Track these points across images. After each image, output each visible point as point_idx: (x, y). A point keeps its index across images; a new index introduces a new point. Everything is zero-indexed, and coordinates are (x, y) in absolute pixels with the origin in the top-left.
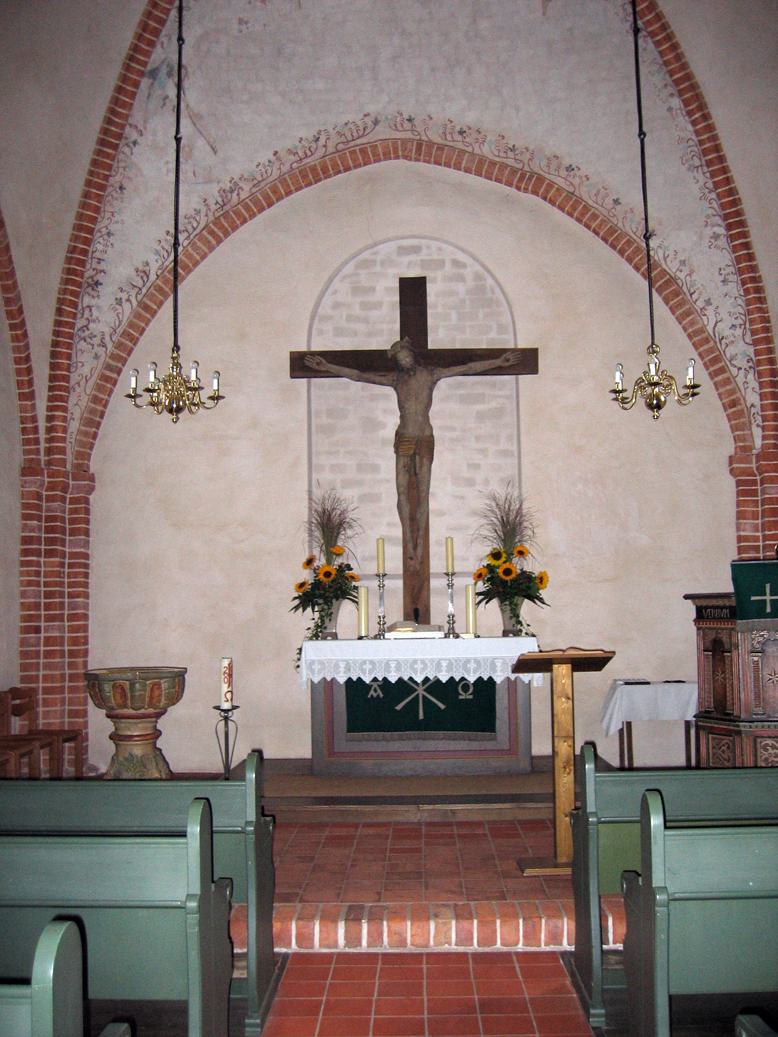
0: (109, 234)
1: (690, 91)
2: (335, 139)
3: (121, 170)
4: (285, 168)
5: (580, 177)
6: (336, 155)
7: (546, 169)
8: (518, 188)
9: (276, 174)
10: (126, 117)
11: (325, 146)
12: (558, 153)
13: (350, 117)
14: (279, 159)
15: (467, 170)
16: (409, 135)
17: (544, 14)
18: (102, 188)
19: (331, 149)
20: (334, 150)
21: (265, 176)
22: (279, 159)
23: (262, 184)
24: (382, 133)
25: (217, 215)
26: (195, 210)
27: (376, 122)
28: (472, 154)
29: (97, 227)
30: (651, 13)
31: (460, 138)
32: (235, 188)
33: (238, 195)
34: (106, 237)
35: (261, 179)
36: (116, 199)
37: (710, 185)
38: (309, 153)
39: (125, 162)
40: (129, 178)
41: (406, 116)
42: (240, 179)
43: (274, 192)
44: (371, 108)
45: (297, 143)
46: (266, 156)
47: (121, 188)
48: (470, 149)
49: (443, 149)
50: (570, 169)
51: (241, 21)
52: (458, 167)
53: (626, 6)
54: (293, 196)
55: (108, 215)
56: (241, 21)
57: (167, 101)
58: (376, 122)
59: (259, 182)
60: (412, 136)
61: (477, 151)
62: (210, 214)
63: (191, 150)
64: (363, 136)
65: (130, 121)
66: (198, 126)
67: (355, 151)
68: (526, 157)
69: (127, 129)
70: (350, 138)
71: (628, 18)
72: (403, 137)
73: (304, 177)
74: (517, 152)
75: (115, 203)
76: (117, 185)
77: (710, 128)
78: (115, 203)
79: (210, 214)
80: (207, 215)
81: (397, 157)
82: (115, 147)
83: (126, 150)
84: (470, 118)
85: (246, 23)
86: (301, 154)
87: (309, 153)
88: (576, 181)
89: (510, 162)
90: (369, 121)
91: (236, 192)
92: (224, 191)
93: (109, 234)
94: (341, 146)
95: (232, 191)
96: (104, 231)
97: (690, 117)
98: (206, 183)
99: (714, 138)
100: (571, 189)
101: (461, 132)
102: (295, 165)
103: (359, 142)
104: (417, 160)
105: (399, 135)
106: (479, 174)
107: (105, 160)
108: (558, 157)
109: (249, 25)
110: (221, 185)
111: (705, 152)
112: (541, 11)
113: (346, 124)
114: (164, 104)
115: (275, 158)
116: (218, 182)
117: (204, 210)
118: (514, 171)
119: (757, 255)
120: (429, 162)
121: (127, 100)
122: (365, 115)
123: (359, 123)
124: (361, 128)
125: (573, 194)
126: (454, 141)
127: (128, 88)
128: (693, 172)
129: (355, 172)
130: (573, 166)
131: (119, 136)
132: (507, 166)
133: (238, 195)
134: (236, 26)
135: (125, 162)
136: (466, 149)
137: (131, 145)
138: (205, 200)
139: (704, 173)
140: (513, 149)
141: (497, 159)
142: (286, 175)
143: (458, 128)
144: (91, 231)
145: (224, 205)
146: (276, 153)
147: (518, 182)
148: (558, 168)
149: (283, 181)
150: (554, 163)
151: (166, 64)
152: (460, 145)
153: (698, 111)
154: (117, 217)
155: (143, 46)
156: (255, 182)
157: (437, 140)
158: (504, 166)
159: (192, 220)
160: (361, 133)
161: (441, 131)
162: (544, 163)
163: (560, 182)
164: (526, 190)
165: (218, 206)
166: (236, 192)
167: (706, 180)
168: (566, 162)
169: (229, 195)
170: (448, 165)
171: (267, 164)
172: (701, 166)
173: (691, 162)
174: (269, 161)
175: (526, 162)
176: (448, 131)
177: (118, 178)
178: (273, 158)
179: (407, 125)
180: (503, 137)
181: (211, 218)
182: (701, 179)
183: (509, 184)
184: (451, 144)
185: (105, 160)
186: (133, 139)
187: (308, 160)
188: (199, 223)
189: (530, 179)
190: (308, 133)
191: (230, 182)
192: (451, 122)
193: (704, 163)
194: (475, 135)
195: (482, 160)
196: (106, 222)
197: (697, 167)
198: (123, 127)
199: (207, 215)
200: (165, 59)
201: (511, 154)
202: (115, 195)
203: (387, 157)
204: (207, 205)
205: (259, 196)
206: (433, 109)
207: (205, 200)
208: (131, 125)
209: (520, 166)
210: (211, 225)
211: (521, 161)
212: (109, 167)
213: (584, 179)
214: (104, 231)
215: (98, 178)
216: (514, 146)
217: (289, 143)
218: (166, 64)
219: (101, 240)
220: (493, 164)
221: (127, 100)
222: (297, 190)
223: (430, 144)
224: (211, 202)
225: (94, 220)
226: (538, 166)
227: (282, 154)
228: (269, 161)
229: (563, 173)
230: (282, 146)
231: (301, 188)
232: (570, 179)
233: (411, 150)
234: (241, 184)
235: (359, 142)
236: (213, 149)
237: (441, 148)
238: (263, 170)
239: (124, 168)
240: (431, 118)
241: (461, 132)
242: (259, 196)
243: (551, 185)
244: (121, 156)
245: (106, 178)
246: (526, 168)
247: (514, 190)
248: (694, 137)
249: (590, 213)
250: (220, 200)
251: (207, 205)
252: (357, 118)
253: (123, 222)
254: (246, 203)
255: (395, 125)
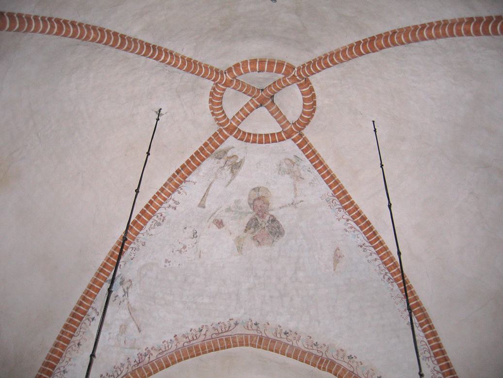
0: (64, 372)
1: (421, 312)
2: (211, 331)
3: (81, 333)
4: (180, 345)
5: (357, 363)
6: (211, 340)
7: (336, 357)
8: (319, 368)
9: (174, 348)
10: (92, 302)
11: (205, 335)
12: (343, 348)
13: (221, 320)
14: (176, 339)
15: (289, 356)
16: (255, 333)
17: (334, 270)
18: (68, 342)
19: (208, 337)
20: (210, 337)
21: (167, 348)
22: (176, 339)
23: (165, 353)
24: (239, 330)
25: (134, 368)
26: (121, 364)
27: (236, 324)
28: (292, 346)
29: (58, 366)
30: (395, 268)
31: (284, 336)
32: (148, 353)
33: (149, 358)
34: (62, 373)
35: (164, 350)
36: (75, 350)
37: (438, 368)
38: (195, 338)
39: (85, 329)
40: (85, 339)
41: (254, 322)
42: (152, 349)
43: (171, 358)
44: (235, 316)
45: (189, 332)
46: (169, 337)
47: (79, 344)
48: (291, 343)
49: (275, 342)
50: (350, 357)
51: (166, 261)
52: (283, 353)
53: (380, 266)
54: (182, 362)
55: (67, 359)
56: (166, 261)
57: (117, 298)
58: (236, 324)
59: (163, 352)
60: (256, 333)
61: (295, 344)
62: (130, 368)
63: (125, 329)
64: (228, 331)
65: (93, 305)
66: (132, 314)
67: (222, 339)
68: (324, 349)
69: (90, 310)
70: (220, 331)
71: (382, 272)
72: (251, 333)
73: (191, 351)
74: (318, 346)
75: (73, 353)
76: (77, 342)
77: (434, 334)
78: (73, 353)
79: (130, 368)
80: (128, 368)
81: (247, 345)
82: (81, 319)
83: (87, 322)
84: (292, 325)
85: (169, 262)
86: (190, 338)
87: (195, 338)
88: (355, 365)
89: (315, 352)
90: (232, 323)
91: (148, 356)
92: (141, 354)
93: (64, 372)
94: (214, 336)
95: (146, 356)
96: (62, 369)
97: (421, 327)
98: (131, 348)
99: (437, 340)
100: (352, 370)
101: (286, 333)
102: (186, 344)
103: (225, 334)
104: (259, 347)
105: (248, 332)
106: (296, 358)
107: (72, 325)
108: (343, 350)
109: (171, 263)
110: (140, 351)
111: (433, 348)
112: (333, 268)
113: (219, 323)
114: (115, 300)
115: (174, 338)
116: (138, 349)
117: (126, 364)
118: (317, 357)
119: (181, 164)
120: (266, 349)
121: (94, 292)
122: (230, 320)
123: (226, 324)
124: (227, 326)
125: (353, 372)
126: (281, 338)
127: (95, 286)
128: (426, 360)
129: (221, 351)
130: (352, 356)
131: (85, 313)
132: (312, 354)
133: (149, 358)
134: (163, 263)
135: (85, 329)
136: (288, 343)
137: (91, 320)
138: (129, 359)
139: (432, 361)
140: (316, 344)
141: (307, 350)
142: (180, 350)
143: (284, 331)
144: (53, 367)
145: (140, 363)
146: (175, 336)
147: (319, 364)
148: (343, 357)
149: (177, 352)
150: (341, 354)
151: (121, 277)
152: (285, 341)
153: (426, 324)
154: (72, 362)
155: (109, 264)
156: (161, 351)
157: (271, 336)
158: (310, 354)
159: (118, 370)
160: (227, 329)
161: (274, 332)
162: (335, 354)
163: (344, 365)
164: (324, 369)
165: (136, 363)
166: (148, 356)
167: (434, 366)
168: (348, 354)
169: (144, 357)
170: (277, 352)
171: (169, 341)
172: (431, 357)
173: (424, 355)
174: (171, 340)
175: (324, 352)
176: (278, 332)
177: (78, 338)
178: (173, 339)
179: (254, 327)
180: (310, 337)
181: (130, 370)
182: (432, 365)
183: (314, 365)
184: (279, 339)
185: (72, 325)
186: (93, 316)
187: (194, 342)
188: (122, 372)
189: (327, 362)
190: (195, 327)
191: (146, 349)
192: (280, 327)
193: (432, 355)
194: (294, 335)
195: (298, 350)
196: (63, 364)
197: (428, 358)
198: (88, 308)
199: (128, 368)
200: (120, 274)
201: (315, 348)
202: (74, 348)
203: (241, 345)
204: (129, 362)
205: (162, 360)
206: (269, 319)
207: (129, 359)
208: (93, 308)
209: (320, 355)
210: (129, 374)
211: (321, 352)
212: (74, 330)
213: (359, 364)
214: (62, 369)
215: (66, 335)
216: (317, 343)
217: (183, 331)
218: (121, 277)
219: (58, 374)
220: (304, 352)
221: (94, 292)
222: (185, 359)
223: (268, 339)
224: (132, 360)
225: (57, 361)
226: (331, 355)
227: (179, 337)
228: (171, 340)
229: (347, 360)
230: (180, 333)
231: (187, 358)
232: (351, 363)
233: (256, 341)
234: (152, 352)
235: (225, 334)
236: (139, 329)
237: (273, 341)
238: (167, 346)
239: (84, 332)
240: (269, 324)
241: (286, 333)
242: (162, 360)
243: (339, 367)
244: (83, 325)
245: (71, 336)
246: (324, 356)
247: (316, 369)
248: (425, 340)
249: (336, 365)
250: (137, 360)
251: (129, 362)
252: (226, 321)
253: (75, 365)
254: (153, 364)
255: (248, 327)
